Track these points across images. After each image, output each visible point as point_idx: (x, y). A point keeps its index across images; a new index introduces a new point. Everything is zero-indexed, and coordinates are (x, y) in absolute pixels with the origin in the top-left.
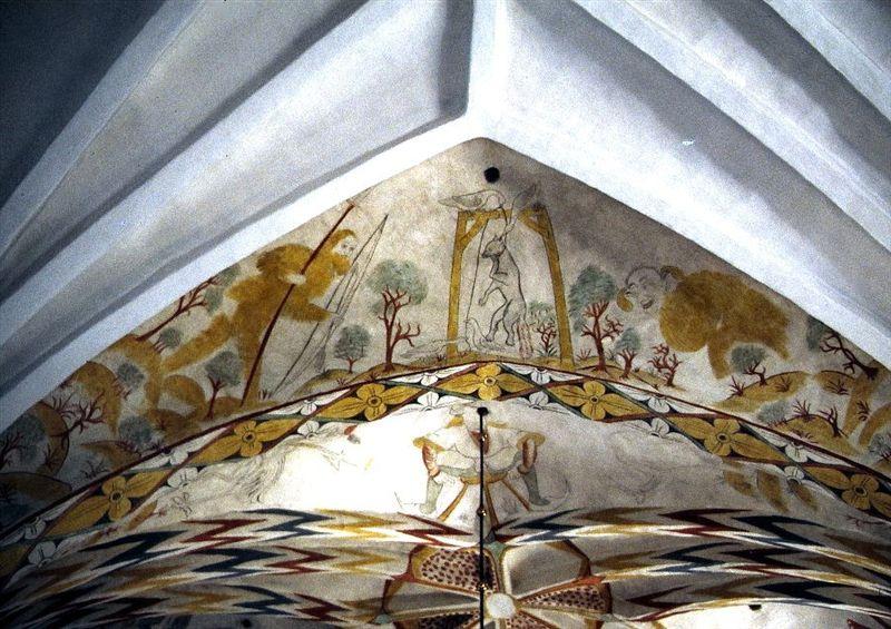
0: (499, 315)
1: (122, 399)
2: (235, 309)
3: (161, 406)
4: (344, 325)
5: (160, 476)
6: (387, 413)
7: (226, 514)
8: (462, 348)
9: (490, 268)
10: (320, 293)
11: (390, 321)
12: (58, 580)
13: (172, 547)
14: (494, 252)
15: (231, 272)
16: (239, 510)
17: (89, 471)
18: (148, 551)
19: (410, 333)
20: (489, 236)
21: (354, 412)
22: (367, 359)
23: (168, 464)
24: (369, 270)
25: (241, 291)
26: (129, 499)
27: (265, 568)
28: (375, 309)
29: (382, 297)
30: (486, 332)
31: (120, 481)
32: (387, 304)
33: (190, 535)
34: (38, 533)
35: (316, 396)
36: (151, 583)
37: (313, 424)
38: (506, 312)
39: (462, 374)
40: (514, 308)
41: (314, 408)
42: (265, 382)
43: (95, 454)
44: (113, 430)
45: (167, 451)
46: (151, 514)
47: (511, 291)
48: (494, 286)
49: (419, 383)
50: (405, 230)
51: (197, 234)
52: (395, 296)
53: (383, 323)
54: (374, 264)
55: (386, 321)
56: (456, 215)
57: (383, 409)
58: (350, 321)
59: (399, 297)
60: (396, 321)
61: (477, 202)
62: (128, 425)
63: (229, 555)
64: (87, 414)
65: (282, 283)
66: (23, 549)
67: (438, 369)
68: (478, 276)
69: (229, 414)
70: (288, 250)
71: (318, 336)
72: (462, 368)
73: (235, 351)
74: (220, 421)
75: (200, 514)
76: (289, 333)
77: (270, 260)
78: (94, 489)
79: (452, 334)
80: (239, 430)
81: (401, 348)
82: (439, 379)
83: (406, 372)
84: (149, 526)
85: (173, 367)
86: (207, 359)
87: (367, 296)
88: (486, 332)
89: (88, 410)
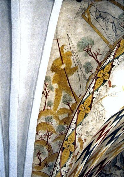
0: (114, 28)
1: (52, 126)
2: (57, 85)
3: (61, 119)
4: (83, 65)
5: (73, 134)
6: (110, 74)
7: (100, 129)
8: (112, 43)
9: (101, 20)
10: (71, 63)
11: (91, 54)
12: (75, 173)
13: (94, 146)
14: (98, 15)
15: (47, 79)
16: (103, 125)
17: (58, 146)
18: (90, 151)
19: (98, 53)
20: (93, 14)
21: (102, 81)
22: (94, 68)
23: (73, 130)
24: (76, 49)
25: (55, 79)
26: (72, 144)
27: (122, 132)
28: (86, 55)
29: (84, 51)
30: (114, 34)
31: (66, 142)
32: (87, 52)
33: (96, 139)
34: (59, 168)
35: (90, 86)
36: (98, 157)
37: (96, 93)
38: (115, 25)
39: (117, 49)
40: (116, 22)
41: (92, 89)
42: (78, 94)
43: (57, 141)
44: (56, 133)
45: (70, 127)
46: (83, 142)
47: (112, 19)
48: (106, 22)
49: (110, 61)
50: (74, 32)
51: (33, 78)
52: (87, 48)
53: (90, 56)
54: (76, 46)
55: (90, 55)
56: (81, 17)
57: (108, 75)
58: (83, 64)
59: (88, 47)
60: (93, 53)
61: (82, 9)
62: (58, 129)
63: (112, 135)
64: (48, 135)
65: (62, 70)
66: (59, 173)
67: (111, 54)
68: (100, 24)
69: (76, 107)
70: (55, 63)
71: (80, 73)
72: (116, 48)
73: (66, 93)
74: (75, 111)
75: (94, 133)
76: (73, 78)
77: (54, 68)
78: (62, 149)
79: (107, 43)
80: (80, 109)
81: (99, 58)
82: (113, 56)
83: (104, 62)
84: (85, 145)
85: (56, 109)
86: (61, 101)
87: (81, 55)
88: (114, 34)
89: (47, 134)
